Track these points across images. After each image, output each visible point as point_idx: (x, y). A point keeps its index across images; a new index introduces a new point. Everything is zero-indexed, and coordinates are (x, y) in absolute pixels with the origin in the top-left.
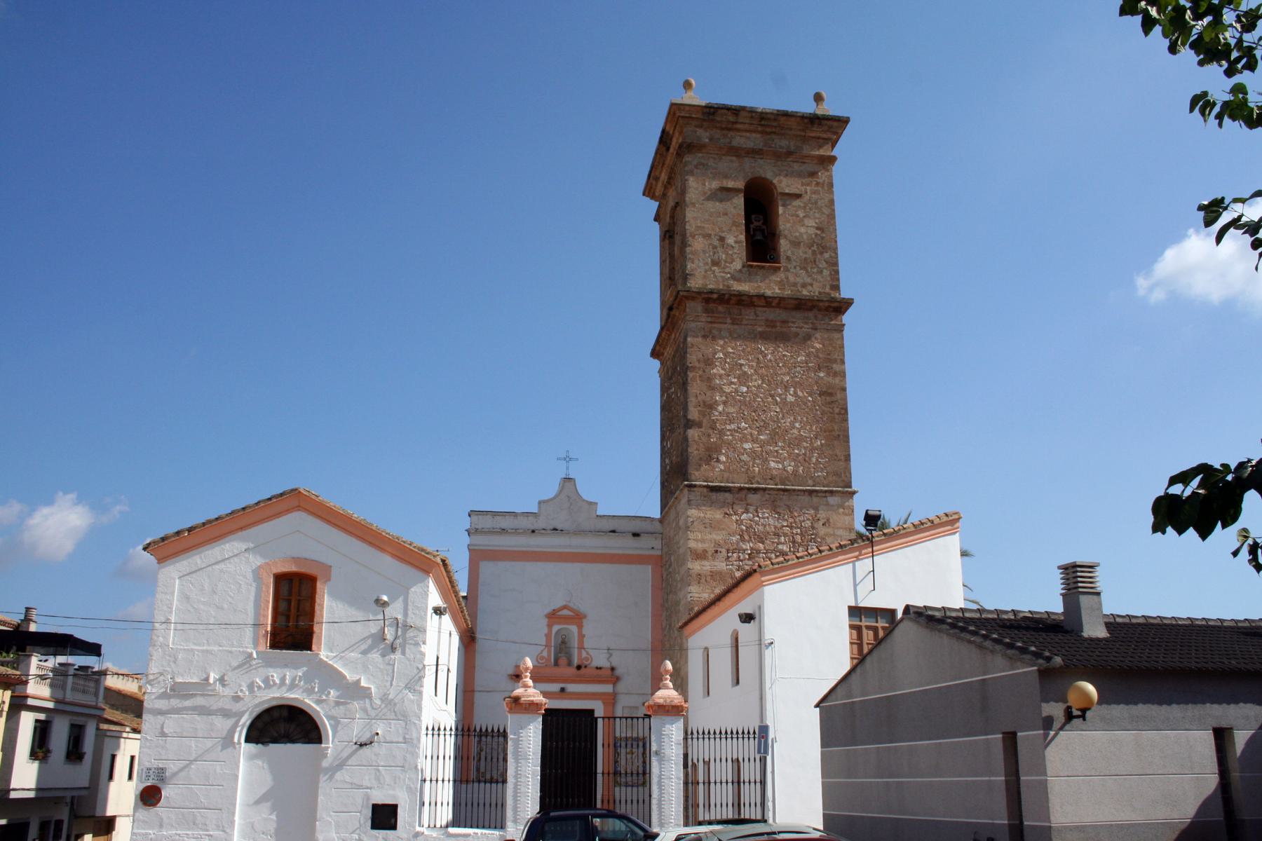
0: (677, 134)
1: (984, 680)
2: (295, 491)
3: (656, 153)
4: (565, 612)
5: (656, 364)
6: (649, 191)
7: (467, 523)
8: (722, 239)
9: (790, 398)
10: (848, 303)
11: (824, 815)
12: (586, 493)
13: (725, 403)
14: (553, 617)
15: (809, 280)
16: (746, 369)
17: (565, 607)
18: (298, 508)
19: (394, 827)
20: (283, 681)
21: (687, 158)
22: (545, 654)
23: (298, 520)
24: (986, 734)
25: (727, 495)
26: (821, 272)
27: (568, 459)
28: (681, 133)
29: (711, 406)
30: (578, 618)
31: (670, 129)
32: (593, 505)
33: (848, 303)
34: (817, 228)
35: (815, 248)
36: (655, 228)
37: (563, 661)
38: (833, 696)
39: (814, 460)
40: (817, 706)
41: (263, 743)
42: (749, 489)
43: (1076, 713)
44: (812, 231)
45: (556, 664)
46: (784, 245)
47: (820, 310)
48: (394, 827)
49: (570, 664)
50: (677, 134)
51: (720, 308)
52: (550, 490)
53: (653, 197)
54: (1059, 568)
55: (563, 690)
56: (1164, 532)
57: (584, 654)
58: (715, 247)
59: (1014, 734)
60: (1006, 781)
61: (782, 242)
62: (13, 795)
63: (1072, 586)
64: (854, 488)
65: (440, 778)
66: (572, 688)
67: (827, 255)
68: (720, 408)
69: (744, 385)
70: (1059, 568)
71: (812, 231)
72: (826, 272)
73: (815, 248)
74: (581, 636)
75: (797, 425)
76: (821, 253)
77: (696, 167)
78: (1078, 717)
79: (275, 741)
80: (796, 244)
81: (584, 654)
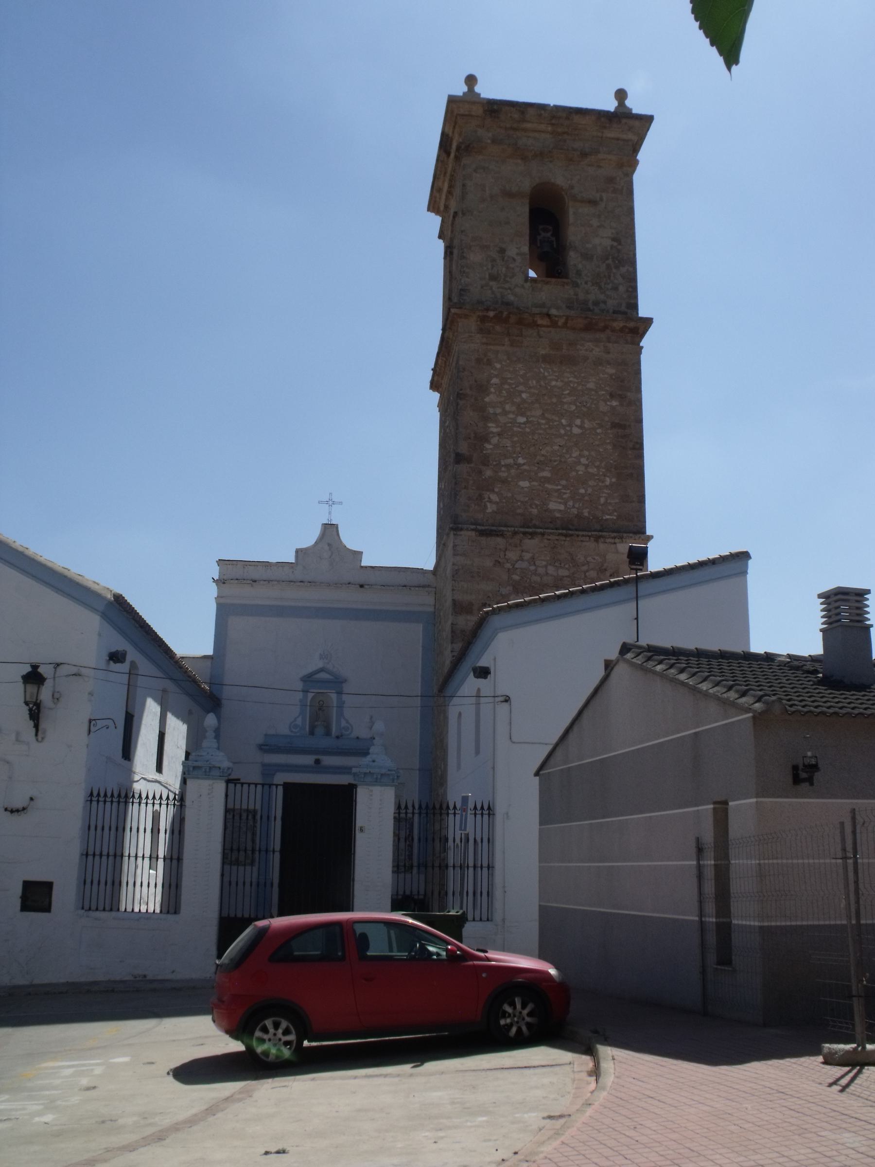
3: (437, 160)
4: (323, 676)
5: (436, 396)
6: (433, 206)
8: (502, 251)
9: (576, 431)
10: (648, 322)
12: (350, 540)
13: (499, 434)
15: (602, 297)
19: (47, 909)
21: (466, 161)
22: (299, 722)
25: (499, 540)
26: (615, 288)
27: (330, 503)
28: (460, 134)
29: (484, 438)
30: (338, 683)
31: (449, 131)
32: (358, 555)
33: (648, 322)
34: (614, 239)
35: (610, 261)
37: (320, 731)
38: (552, 761)
39: (602, 500)
40: (537, 774)
42: (525, 533)
44: (608, 243)
45: (312, 733)
46: (573, 259)
47: (613, 330)
48: (47, 909)
49: (328, 733)
51: (498, 328)
52: (309, 538)
55: (317, 762)
56: (642, 347)
57: (343, 723)
58: (494, 260)
59: (726, 803)
62: (158, 911)
63: (834, 618)
66: (329, 761)
67: (623, 270)
68: (495, 440)
69: (522, 415)
71: (608, 243)
72: (622, 289)
73: (610, 261)
74: (341, 706)
76: (617, 267)
77: (475, 171)
80: (587, 256)
81: (343, 723)
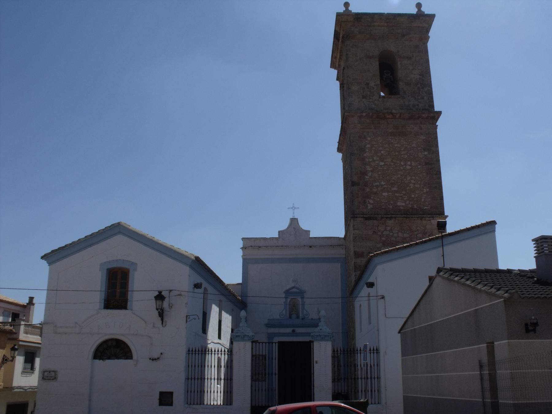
0: (342, 31)
1: (476, 310)
2: (119, 225)
4: (294, 290)
5: (340, 155)
7: (241, 244)
8: (367, 84)
9: (408, 167)
10: (439, 113)
11: (404, 396)
12: (304, 225)
13: (372, 171)
14: (287, 292)
16: (382, 152)
17: (293, 288)
18: (119, 233)
19: (171, 404)
20: (115, 324)
22: (284, 312)
23: (120, 238)
24: (479, 345)
25: (375, 221)
26: (423, 98)
27: (294, 208)
28: (343, 30)
29: (365, 173)
30: (301, 293)
32: (308, 232)
33: (439, 113)
34: (420, 75)
36: (338, 84)
41: (103, 359)
42: (387, 218)
43: (531, 328)
45: (290, 317)
46: (401, 85)
48: (171, 404)
49: (298, 317)
50: (342, 31)
52: (284, 226)
53: (335, 68)
54: (533, 240)
55: (293, 331)
57: (305, 312)
60: (489, 374)
61: (401, 83)
63: (541, 251)
64: (446, 214)
65: (196, 378)
66: (299, 330)
67: (426, 89)
68: (370, 174)
69: (382, 161)
70: (533, 240)
72: (426, 98)
73: (419, 85)
74: (303, 304)
75: (413, 181)
78: (531, 331)
79: (109, 358)
81: (305, 312)
